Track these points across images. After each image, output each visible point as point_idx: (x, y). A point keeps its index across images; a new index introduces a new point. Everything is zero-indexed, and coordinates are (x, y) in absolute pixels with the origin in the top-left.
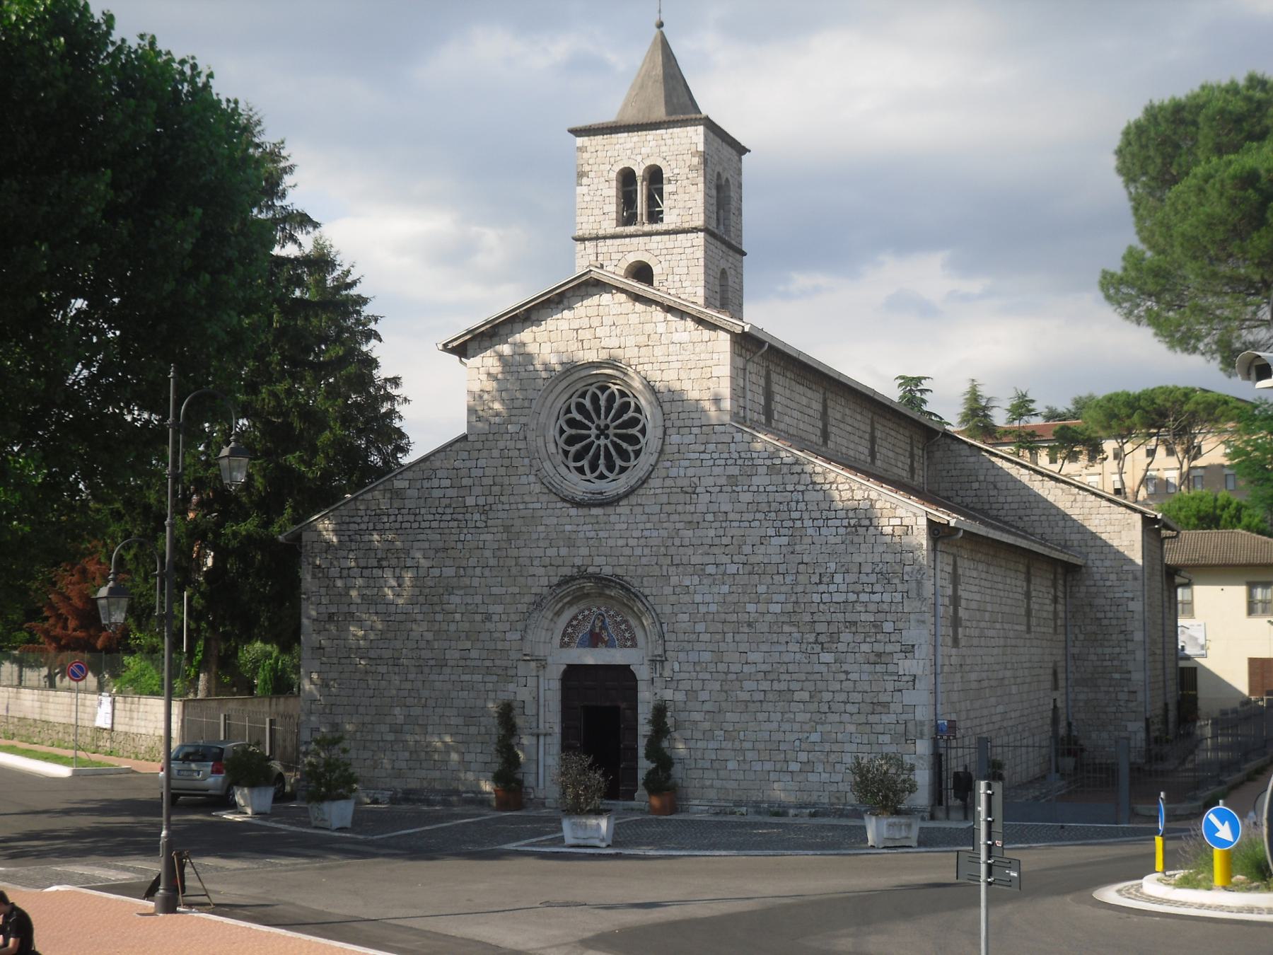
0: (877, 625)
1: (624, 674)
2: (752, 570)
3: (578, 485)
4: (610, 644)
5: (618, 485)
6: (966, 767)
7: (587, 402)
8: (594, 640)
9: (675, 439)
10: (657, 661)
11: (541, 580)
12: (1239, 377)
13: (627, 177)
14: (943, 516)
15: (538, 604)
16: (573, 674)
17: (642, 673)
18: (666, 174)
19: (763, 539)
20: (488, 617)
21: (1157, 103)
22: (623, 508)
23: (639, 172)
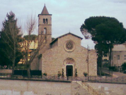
0: (93, 62)
1: (71, 66)
2: (83, 58)
3: (68, 50)
4: (70, 64)
5: (71, 50)
6: (125, 59)
7: (68, 44)
8: (69, 63)
9: (76, 47)
10: (75, 65)
11: (65, 58)
12: (95, 45)
13: (44, 19)
14: (98, 54)
15: (64, 60)
16: (67, 66)
17: (73, 66)
18: (48, 20)
19: (84, 55)
20: (60, 61)
21: (123, 24)
22: (72, 53)
23: (45, 19)
